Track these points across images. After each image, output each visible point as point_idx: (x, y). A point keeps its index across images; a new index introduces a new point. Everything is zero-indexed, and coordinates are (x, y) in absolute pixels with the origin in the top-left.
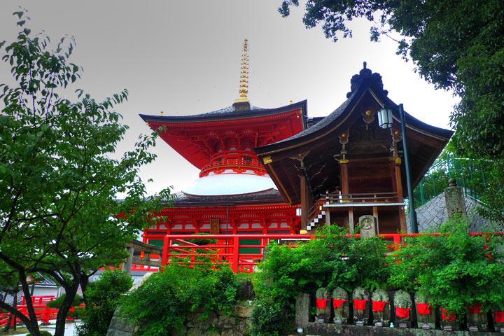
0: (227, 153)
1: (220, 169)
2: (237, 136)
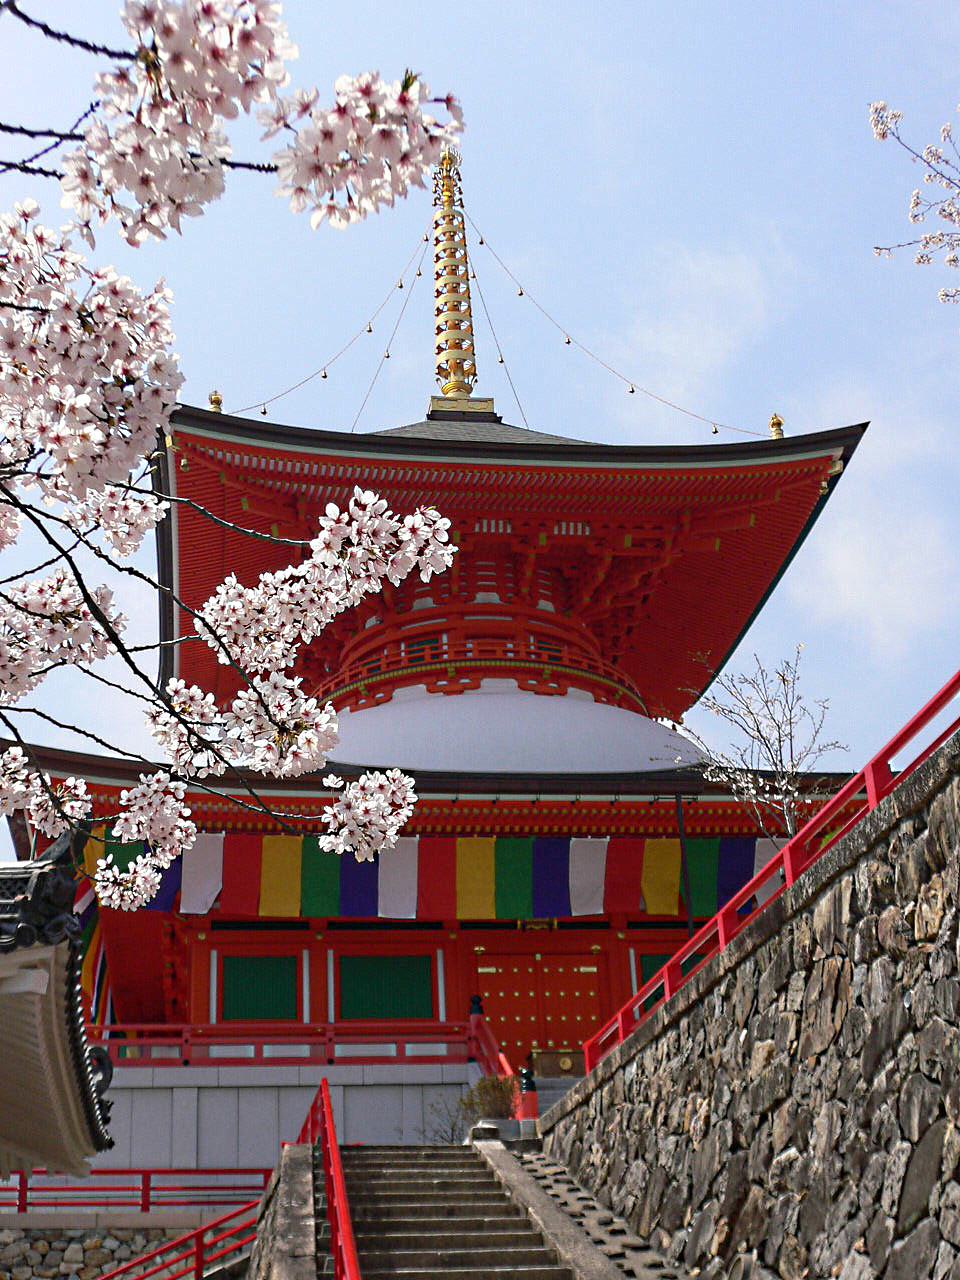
0: (463, 614)
1: (372, 689)
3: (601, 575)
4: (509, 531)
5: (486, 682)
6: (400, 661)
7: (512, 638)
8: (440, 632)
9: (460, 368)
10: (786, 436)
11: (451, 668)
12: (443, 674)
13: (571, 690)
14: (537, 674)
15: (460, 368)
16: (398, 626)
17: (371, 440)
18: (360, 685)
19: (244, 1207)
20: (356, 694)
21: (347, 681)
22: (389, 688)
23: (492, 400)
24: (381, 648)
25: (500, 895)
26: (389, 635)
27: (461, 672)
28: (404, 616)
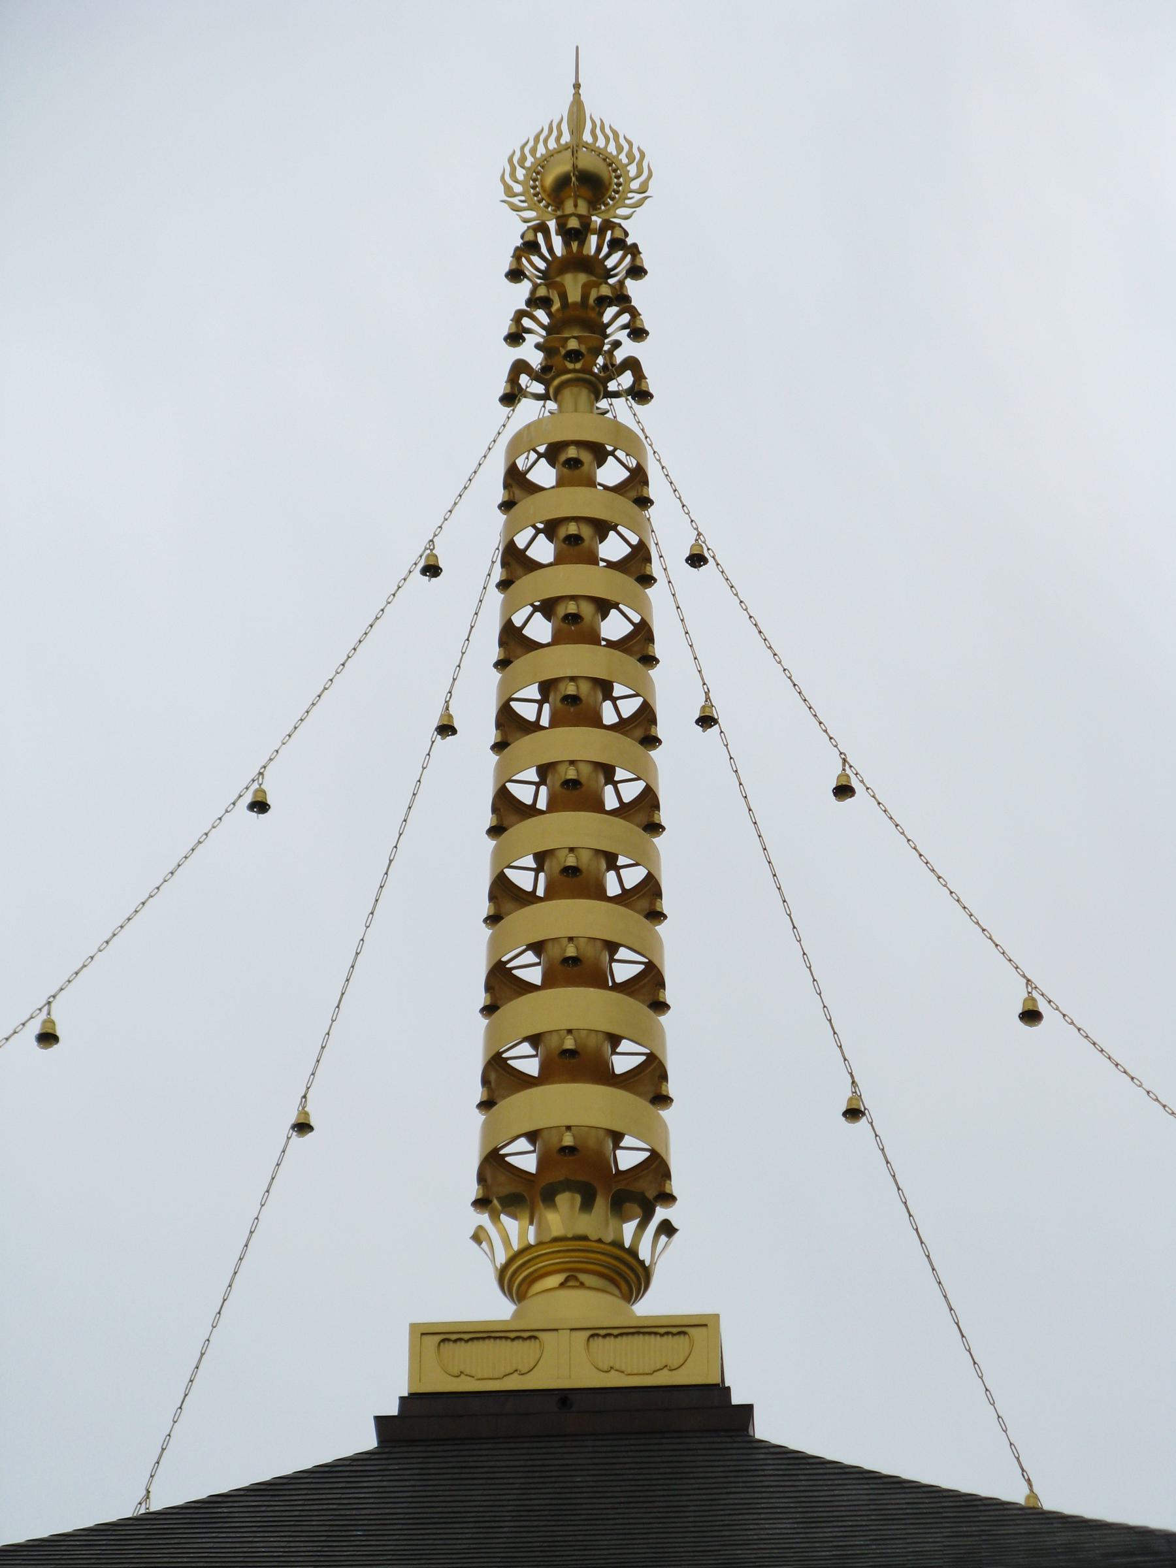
9: (578, 1180)
15: (578, 1180)
23: (706, 1325)
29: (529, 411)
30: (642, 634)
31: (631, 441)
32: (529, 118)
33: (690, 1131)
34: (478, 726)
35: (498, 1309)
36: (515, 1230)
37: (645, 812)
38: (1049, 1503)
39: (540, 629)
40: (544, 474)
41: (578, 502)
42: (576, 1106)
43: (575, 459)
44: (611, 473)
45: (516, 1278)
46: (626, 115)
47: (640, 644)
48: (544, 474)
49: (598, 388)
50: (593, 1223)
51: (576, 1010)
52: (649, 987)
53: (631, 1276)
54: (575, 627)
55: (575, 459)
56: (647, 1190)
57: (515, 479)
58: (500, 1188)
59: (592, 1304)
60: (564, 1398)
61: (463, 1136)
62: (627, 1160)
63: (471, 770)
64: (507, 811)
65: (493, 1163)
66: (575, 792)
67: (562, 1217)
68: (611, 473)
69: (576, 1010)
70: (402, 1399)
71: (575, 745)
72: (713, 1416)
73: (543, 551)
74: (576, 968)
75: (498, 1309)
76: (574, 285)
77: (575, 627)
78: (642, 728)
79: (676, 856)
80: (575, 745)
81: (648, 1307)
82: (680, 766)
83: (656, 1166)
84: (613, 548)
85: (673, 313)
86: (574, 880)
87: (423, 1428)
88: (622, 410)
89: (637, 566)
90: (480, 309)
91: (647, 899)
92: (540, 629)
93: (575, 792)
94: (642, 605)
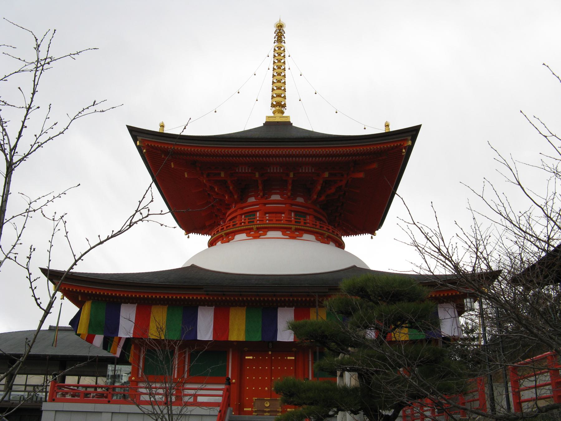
0: (265, 204)
1: (227, 234)
2: (257, 175)
3: (319, 187)
4: (281, 171)
5: (306, 236)
6: (291, 221)
7: (284, 213)
8: (256, 211)
9: (279, 105)
10: (391, 130)
11: (294, 227)
12: (251, 229)
13: (331, 243)
14: (322, 235)
15: (279, 105)
16: (242, 208)
17: (234, 138)
18: (223, 233)
19: (36, 84)
20: (221, 236)
21: (225, 229)
22: (233, 234)
23: (289, 117)
24: (236, 217)
25: (247, 331)
26: (239, 212)
27: (297, 230)
28: (243, 205)
29: (276, 44)
30: (284, 62)
31: (284, 47)
32: (276, 21)
33: (288, 102)
34: (271, 69)
35: (273, 115)
36: (274, 109)
37: (284, 76)
38: (150, 180)
39: (276, 61)
40: (277, 49)
41: (279, 51)
42: (278, 99)
43: (279, 48)
44: (282, 49)
45: (274, 113)
46: (283, 21)
47: (284, 63)
48: (277, 49)
49: (281, 42)
50: (280, 108)
51: (279, 92)
52: (285, 90)
53: (283, 113)
54: (279, 61)
55: (279, 48)
56: (284, 106)
57: (275, 49)
58: (273, 105)
59: (280, 115)
60: (278, 122)
61: (269, 101)
62: (283, 103)
63: (271, 72)
64: (274, 76)
65: (272, 103)
66: (279, 74)
67: (277, 108)
68: (282, 49)
69: (279, 92)
70: (373, 233)
71: (279, 71)
72: (289, 124)
73: (277, 55)
74: (279, 88)
75: (273, 115)
76: (280, 34)
77: (279, 61)
78: (284, 69)
79: (287, 80)
80: (279, 71)
81: (284, 115)
82: (287, 72)
83: (285, 104)
84: (282, 55)
85: (287, 37)
86: (279, 81)
87: (267, 124)
88: (283, 44)
89: (284, 56)
90: (272, 36)
91: (284, 83)
92: (276, 61)
93: (279, 74)
94: (285, 101)
